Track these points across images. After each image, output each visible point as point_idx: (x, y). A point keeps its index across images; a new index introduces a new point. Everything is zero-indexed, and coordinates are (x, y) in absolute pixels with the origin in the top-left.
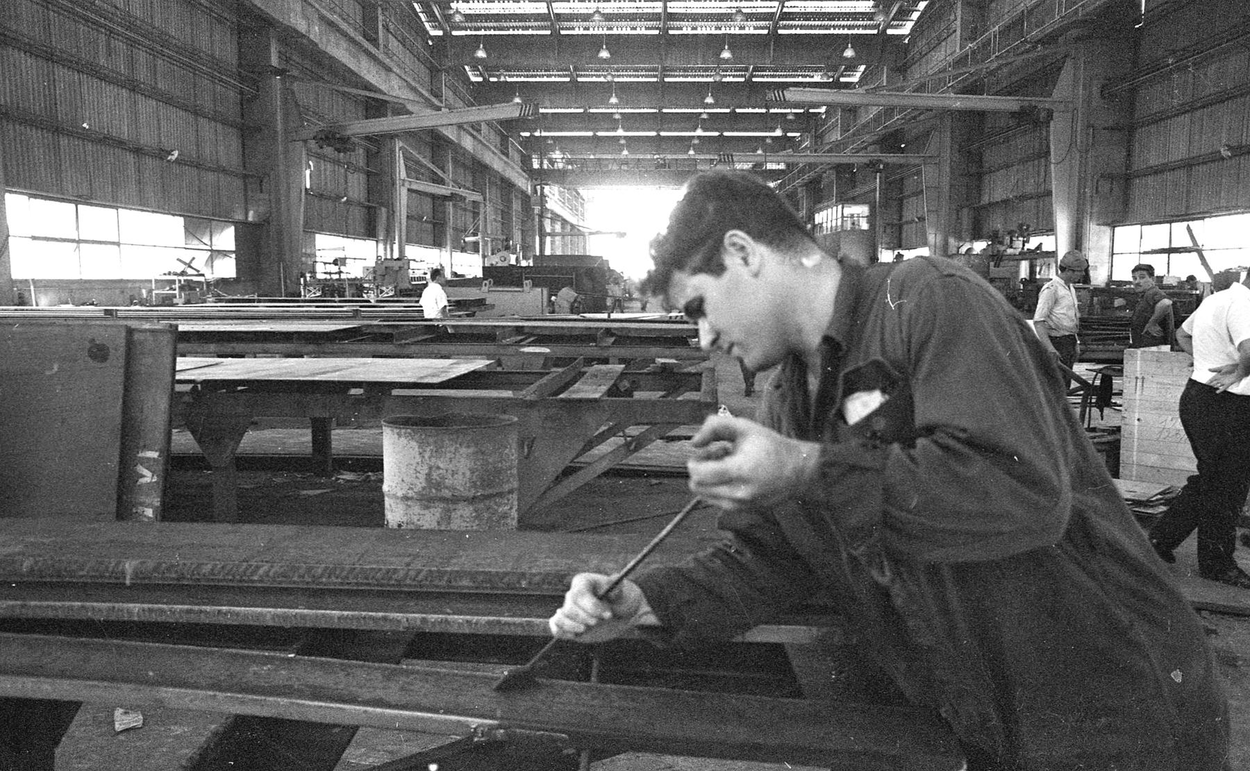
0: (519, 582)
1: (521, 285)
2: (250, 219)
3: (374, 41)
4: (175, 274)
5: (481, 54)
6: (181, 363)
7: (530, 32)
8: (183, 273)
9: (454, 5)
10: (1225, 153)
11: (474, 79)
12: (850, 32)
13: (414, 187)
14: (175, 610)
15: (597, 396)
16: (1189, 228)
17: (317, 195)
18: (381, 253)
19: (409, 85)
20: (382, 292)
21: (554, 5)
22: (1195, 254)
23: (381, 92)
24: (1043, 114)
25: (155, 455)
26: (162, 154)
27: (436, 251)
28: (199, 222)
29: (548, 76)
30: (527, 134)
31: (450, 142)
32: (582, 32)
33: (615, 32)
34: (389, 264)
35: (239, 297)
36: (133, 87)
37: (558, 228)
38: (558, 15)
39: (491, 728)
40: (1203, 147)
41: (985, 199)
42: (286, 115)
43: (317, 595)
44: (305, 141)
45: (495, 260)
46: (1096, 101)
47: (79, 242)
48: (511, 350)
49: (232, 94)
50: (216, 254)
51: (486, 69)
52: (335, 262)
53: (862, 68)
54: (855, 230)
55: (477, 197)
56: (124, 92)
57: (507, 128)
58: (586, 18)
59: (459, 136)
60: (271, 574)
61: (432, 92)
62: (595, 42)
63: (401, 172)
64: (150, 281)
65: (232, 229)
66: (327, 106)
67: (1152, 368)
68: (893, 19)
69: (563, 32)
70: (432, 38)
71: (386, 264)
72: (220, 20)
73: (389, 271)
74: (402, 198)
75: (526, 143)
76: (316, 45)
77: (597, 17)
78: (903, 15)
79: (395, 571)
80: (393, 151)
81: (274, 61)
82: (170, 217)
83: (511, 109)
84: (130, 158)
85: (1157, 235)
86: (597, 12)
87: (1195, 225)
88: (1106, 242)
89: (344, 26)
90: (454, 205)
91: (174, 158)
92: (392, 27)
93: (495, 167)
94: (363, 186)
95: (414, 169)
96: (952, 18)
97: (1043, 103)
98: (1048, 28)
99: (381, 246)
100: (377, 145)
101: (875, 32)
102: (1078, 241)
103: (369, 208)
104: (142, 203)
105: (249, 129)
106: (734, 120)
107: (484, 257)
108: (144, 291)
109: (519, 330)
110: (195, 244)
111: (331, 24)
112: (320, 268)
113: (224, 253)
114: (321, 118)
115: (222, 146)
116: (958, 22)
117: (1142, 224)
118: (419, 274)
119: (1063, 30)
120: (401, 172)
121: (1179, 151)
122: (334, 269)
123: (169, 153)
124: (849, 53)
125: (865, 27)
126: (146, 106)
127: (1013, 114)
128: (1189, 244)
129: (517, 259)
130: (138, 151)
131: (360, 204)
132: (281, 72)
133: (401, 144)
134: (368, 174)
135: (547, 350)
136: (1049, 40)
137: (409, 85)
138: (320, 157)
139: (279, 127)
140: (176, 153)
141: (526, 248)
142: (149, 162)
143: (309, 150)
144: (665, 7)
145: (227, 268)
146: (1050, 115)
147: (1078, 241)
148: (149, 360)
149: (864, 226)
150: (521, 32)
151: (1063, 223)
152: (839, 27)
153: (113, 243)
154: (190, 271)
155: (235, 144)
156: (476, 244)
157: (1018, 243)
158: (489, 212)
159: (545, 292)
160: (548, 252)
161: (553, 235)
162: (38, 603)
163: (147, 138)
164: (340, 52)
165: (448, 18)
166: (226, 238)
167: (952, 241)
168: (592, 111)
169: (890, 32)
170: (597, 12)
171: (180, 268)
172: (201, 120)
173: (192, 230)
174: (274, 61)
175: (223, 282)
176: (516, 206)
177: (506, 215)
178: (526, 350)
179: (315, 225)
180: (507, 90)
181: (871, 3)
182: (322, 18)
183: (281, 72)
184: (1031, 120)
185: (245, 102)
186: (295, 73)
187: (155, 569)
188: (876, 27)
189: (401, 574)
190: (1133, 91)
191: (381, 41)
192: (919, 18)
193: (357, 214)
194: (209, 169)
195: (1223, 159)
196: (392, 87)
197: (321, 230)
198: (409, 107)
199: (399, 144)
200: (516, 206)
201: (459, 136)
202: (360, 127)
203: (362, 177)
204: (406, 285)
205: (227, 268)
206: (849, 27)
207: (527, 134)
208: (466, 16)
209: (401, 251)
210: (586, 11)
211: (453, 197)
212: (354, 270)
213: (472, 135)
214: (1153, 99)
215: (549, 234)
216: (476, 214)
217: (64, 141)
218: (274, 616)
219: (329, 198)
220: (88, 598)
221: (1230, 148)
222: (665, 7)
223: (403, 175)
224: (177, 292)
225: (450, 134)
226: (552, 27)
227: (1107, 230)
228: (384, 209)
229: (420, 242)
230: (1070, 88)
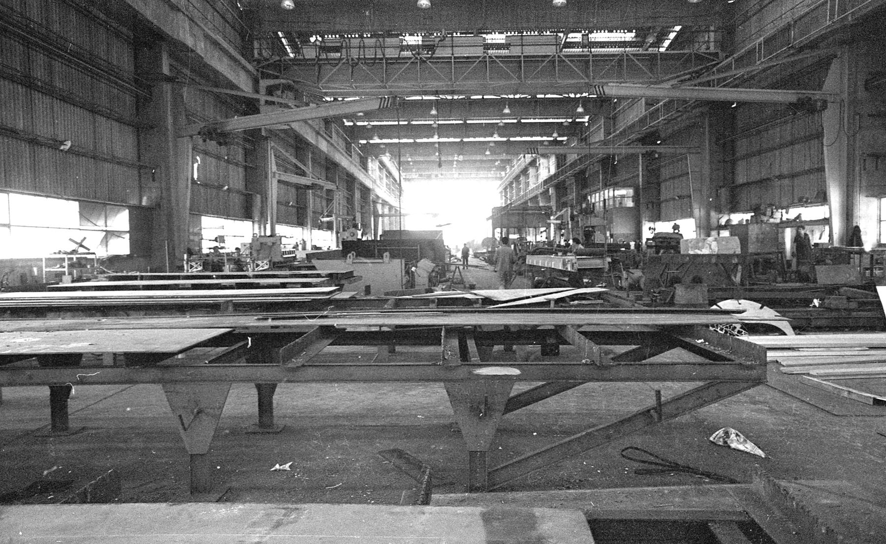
2: (144, 203)
4: (65, 253)
8: (74, 252)
13: (283, 178)
18: (257, 231)
20: (258, 265)
24: (819, 104)
26: (55, 144)
27: (299, 229)
28: (93, 204)
30: (364, 142)
34: (263, 240)
37: (386, 211)
41: (741, 179)
44: (191, 137)
45: (347, 236)
46: (862, 94)
49: (128, 97)
50: (109, 234)
54: (623, 209)
63: (273, 167)
64: (41, 260)
65: (127, 211)
72: (118, 34)
73: (263, 246)
74: (274, 190)
75: (363, 148)
76: (202, 58)
81: (166, 70)
84: (25, 148)
89: (225, 45)
90: (314, 195)
91: (67, 147)
93: (343, 164)
95: (283, 165)
97: (817, 95)
98: (814, 33)
99: (256, 226)
100: (254, 137)
102: (848, 213)
104: (37, 188)
106: (521, 128)
107: (337, 233)
108: (35, 270)
110: (90, 226)
111: (215, 44)
118: (289, 248)
119: (823, 38)
120: (273, 167)
123: (62, 143)
130: (34, 142)
131: (238, 192)
138: (206, 153)
142: (45, 154)
145: (122, 247)
146: (825, 106)
147: (848, 213)
149: (630, 204)
151: (835, 196)
153: (4, 225)
154: (81, 250)
157: (777, 215)
158: (339, 197)
161: (383, 216)
166: (121, 220)
167: (713, 214)
168: (414, 123)
171: (74, 246)
172: (99, 119)
174: (166, 70)
175: (114, 260)
176: (357, 195)
177: (350, 200)
179: (197, 212)
181: (633, 35)
182: (207, 37)
183: (169, 79)
193: (236, 200)
194: (105, 160)
199: (271, 144)
200: (357, 195)
201: (317, 141)
202: (239, 123)
203: (241, 170)
204: (277, 259)
205: (122, 247)
207: (364, 142)
209: (273, 229)
211: (313, 186)
212: (230, 247)
213: (326, 140)
216: (329, 201)
223: (274, 168)
224: (66, 270)
229: (288, 223)
230: (836, 82)
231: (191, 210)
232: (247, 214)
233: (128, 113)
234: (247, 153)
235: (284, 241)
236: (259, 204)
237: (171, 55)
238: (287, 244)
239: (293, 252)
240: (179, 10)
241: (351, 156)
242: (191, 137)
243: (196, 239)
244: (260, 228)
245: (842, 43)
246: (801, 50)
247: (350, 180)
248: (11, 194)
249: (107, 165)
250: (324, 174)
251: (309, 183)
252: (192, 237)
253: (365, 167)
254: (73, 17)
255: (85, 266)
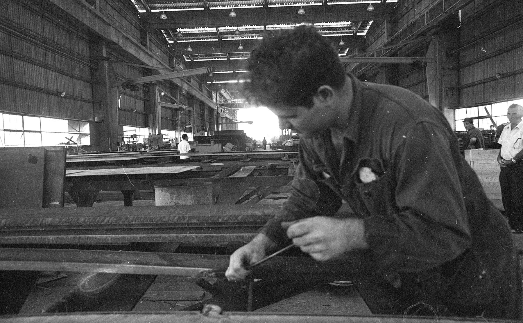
0: (218, 220)
1: (210, 143)
2: (96, 120)
3: (145, 45)
4: (65, 144)
5: (190, 49)
6: (67, 172)
7: (210, 40)
8: (68, 143)
9: (178, 30)
10: (498, 77)
11: (187, 60)
12: (342, 35)
13: (164, 105)
14: (69, 238)
15: (245, 176)
16: (485, 108)
17: (123, 110)
18: (151, 132)
19: (160, 63)
20: (152, 148)
21: (219, 28)
22: (489, 119)
23: (148, 65)
25: (57, 203)
26: (58, 94)
28: (75, 119)
29: (218, 58)
30: (210, 83)
31: (178, 86)
32: (231, 39)
33: (245, 38)
35: (92, 152)
36: (46, 66)
37: (224, 121)
38: (221, 33)
39: (210, 272)
40: (487, 76)
42: (110, 77)
43: (130, 229)
44: (118, 87)
45: (198, 134)
47: (24, 131)
48: (208, 164)
51: (192, 56)
52: (132, 137)
53: (348, 50)
55: (190, 109)
56: (43, 69)
57: (202, 79)
58: (232, 33)
59: (182, 84)
60: (110, 222)
61: (170, 66)
62: (237, 43)
66: (125, 72)
67: (477, 157)
68: (359, 29)
69: (223, 40)
70: (169, 44)
71: (153, 136)
72: (82, 39)
74: (159, 110)
77: (237, 32)
78: (363, 27)
79: (164, 217)
80: (154, 91)
81: (104, 55)
82: (62, 120)
83: (202, 71)
84: (45, 97)
85: (472, 112)
86: (237, 30)
87: (488, 107)
88: (452, 115)
89: (133, 40)
92: (153, 40)
94: (143, 106)
96: (383, 27)
98: (423, 28)
99: (151, 131)
100: (148, 87)
101: (352, 34)
103: (145, 114)
104: (50, 114)
105: (95, 81)
107: (194, 133)
109: (210, 157)
111: (127, 39)
112: (126, 140)
113: (86, 135)
114: (124, 78)
115: (83, 90)
116: (386, 29)
117: (466, 108)
118: (167, 140)
121: (479, 77)
122: (131, 140)
123: (61, 93)
124: (342, 43)
125: (348, 33)
126: (52, 75)
127: (410, 64)
128: (486, 114)
129: (208, 134)
130: (48, 93)
131: (141, 113)
132: (108, 59)
133: (158, 87)
134: (144, 100)
135: (223, 164)
136: (424, 33)
137: (160, 63)
138: (124, 94)
139: (107, 81)
140: (64, 94)
141: (211, 129)
142: (53, 98)
143: (119, 91)
144: (265, 28)
145: (86, 141)
146: (426, 64)
148: (54, 163)
150: (206, 40)
152: (337, 33)
154: (71, 142)
155: (89, 89)
156: (190, 128)
158: (195, 115)
159: (220, 145)
160: (220, 130)
162: (8, 237)
163: (52, 88)
164: (132, 50)
165: (176, 35)
166: (86, 129)
169: (358, 34)
170: (237, 30)
171: (67, 141)
173: (71, 126)
174: (104, 55)
176: (206, 112)
177: (202, 116)
178: (213, 164)
179: (122, 124)
180: (201, 64)
181: (350, 23)
182: (123, 36)
183: (108, 59)
184: (418, 67)
185: (93, 71)
186: (113, 59)
187: (60, 222)
188: (353, 32)
189: (167, 218)
190: (459, 53)
191: (148, 46)
192: (370, 28)
193: (140, 118)
195: (497, 79)
196: (152, 64)
197: (126, 124)
198: (161, 71)
199: (157, 88)
200: (206, 112)
201: (182, 84)
203: (142, 102)
204: (161, 145)
205: (86, 141)
206: (341, 33)
207: (210, 83)
208: (183, 34)
209: (159, 131)
210: (232, 31)
212: (140, 141)
213: (187, 83)
214: (467, 56)
215: (221, 124)
216: (190, 116)
217: (17, 90)
218: (112, 239)
219: (128, 111)
220: (31, 235)
221: (500, 75)
222: (265, 28)
223: (159, 100)
225: (178, 82)
226: (218, 38)
227: (452, 110)
228: (151, 115)
230: (433, 54)
231: (119, 123)
232: (146, 125)
233: (87, 74)
234: (144, 92)
235: (164, 137)
236: (152, 119)
237: (106, 46)
238: (166, 139)
239: (169, 142)
240: (110, 25)
241: (202, 91)
242: (118, 87)
243: (121, 137)
244: (153, 131)
245: (434, 34)
246: (418, 36)
247: (202, 104)
248: (41, 118)
249: (79, 102)
250: (187, 101)
251: (178, 107)
252: (118, 137)
253: (210, 97)
254: (63, 33)
255: (73, 150)
